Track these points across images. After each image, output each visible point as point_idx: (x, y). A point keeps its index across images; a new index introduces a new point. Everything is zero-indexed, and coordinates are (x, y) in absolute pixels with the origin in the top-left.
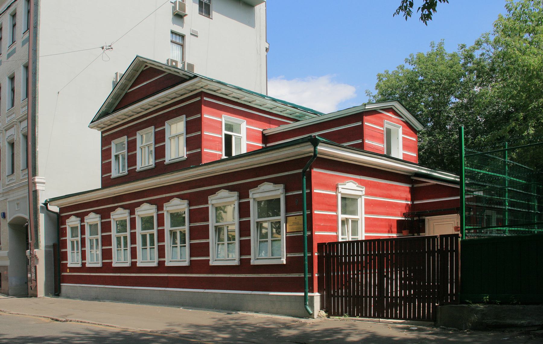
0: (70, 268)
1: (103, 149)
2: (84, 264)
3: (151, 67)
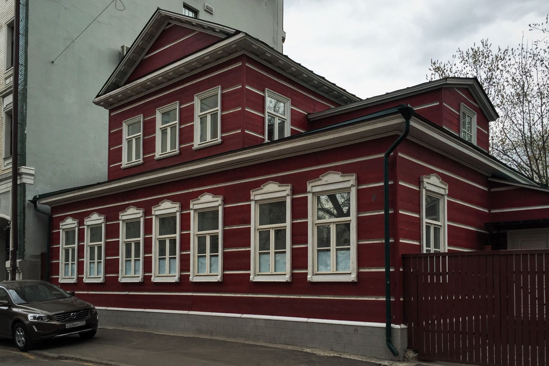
1: (111, 132)
2: (80, 279)
3: (175, 25)
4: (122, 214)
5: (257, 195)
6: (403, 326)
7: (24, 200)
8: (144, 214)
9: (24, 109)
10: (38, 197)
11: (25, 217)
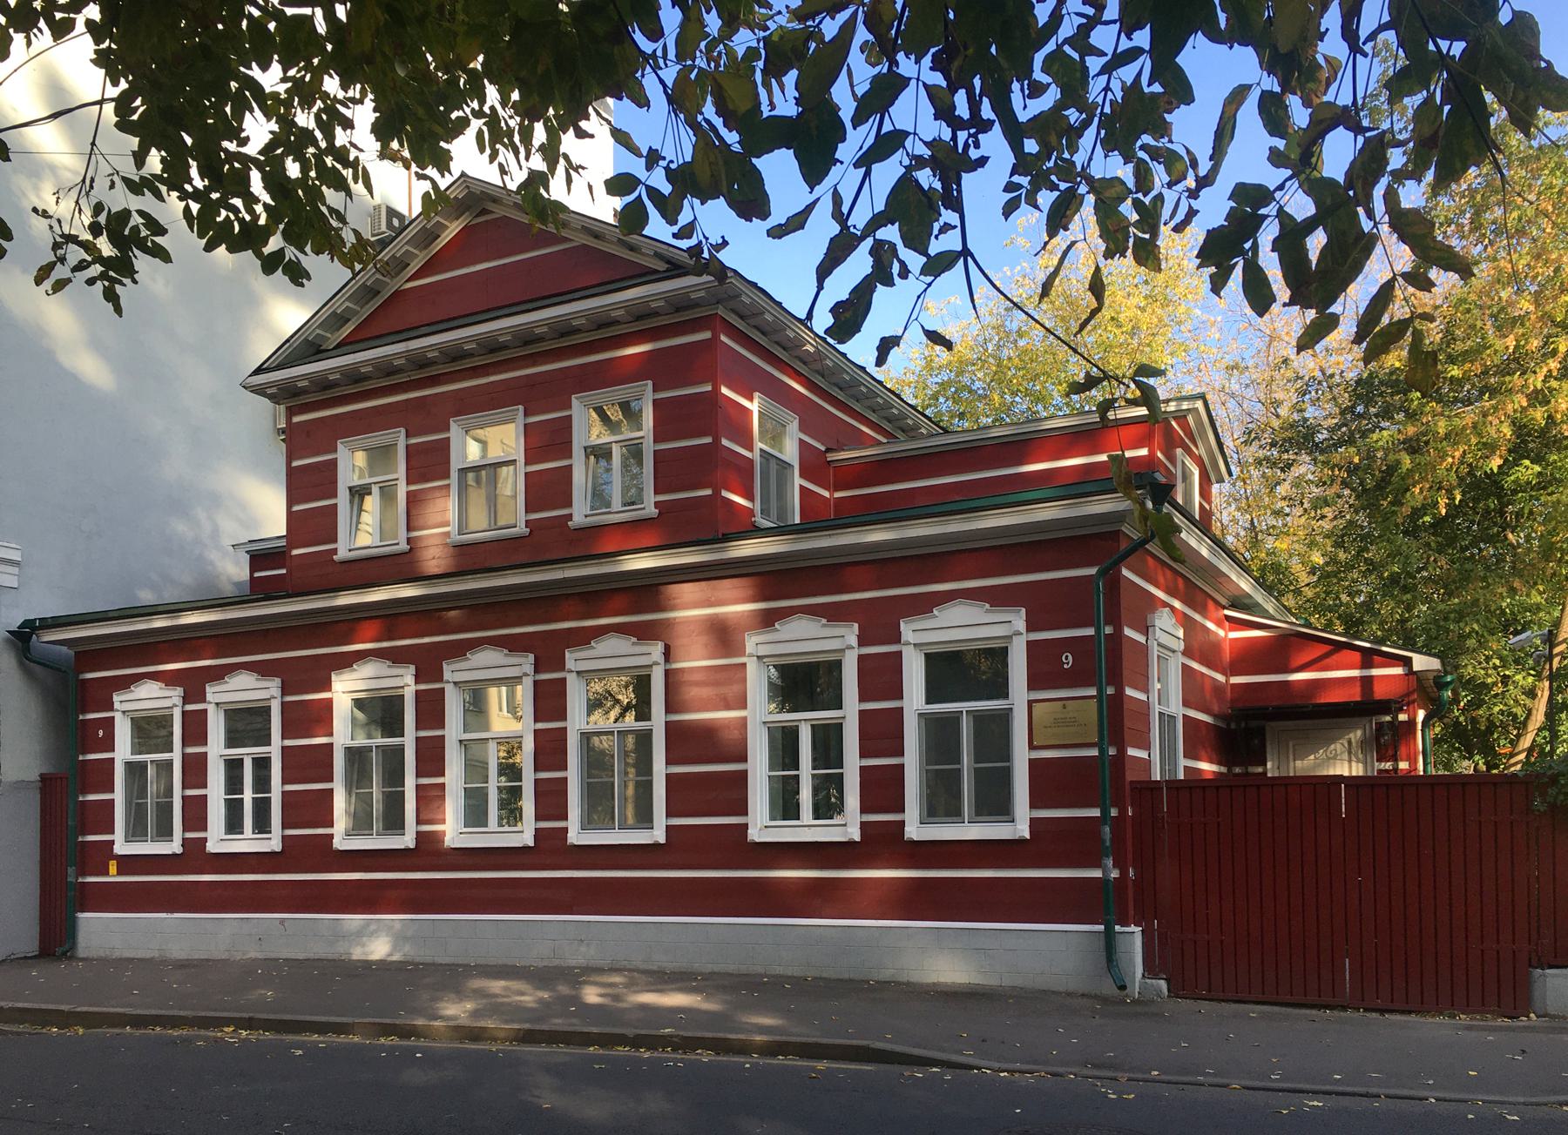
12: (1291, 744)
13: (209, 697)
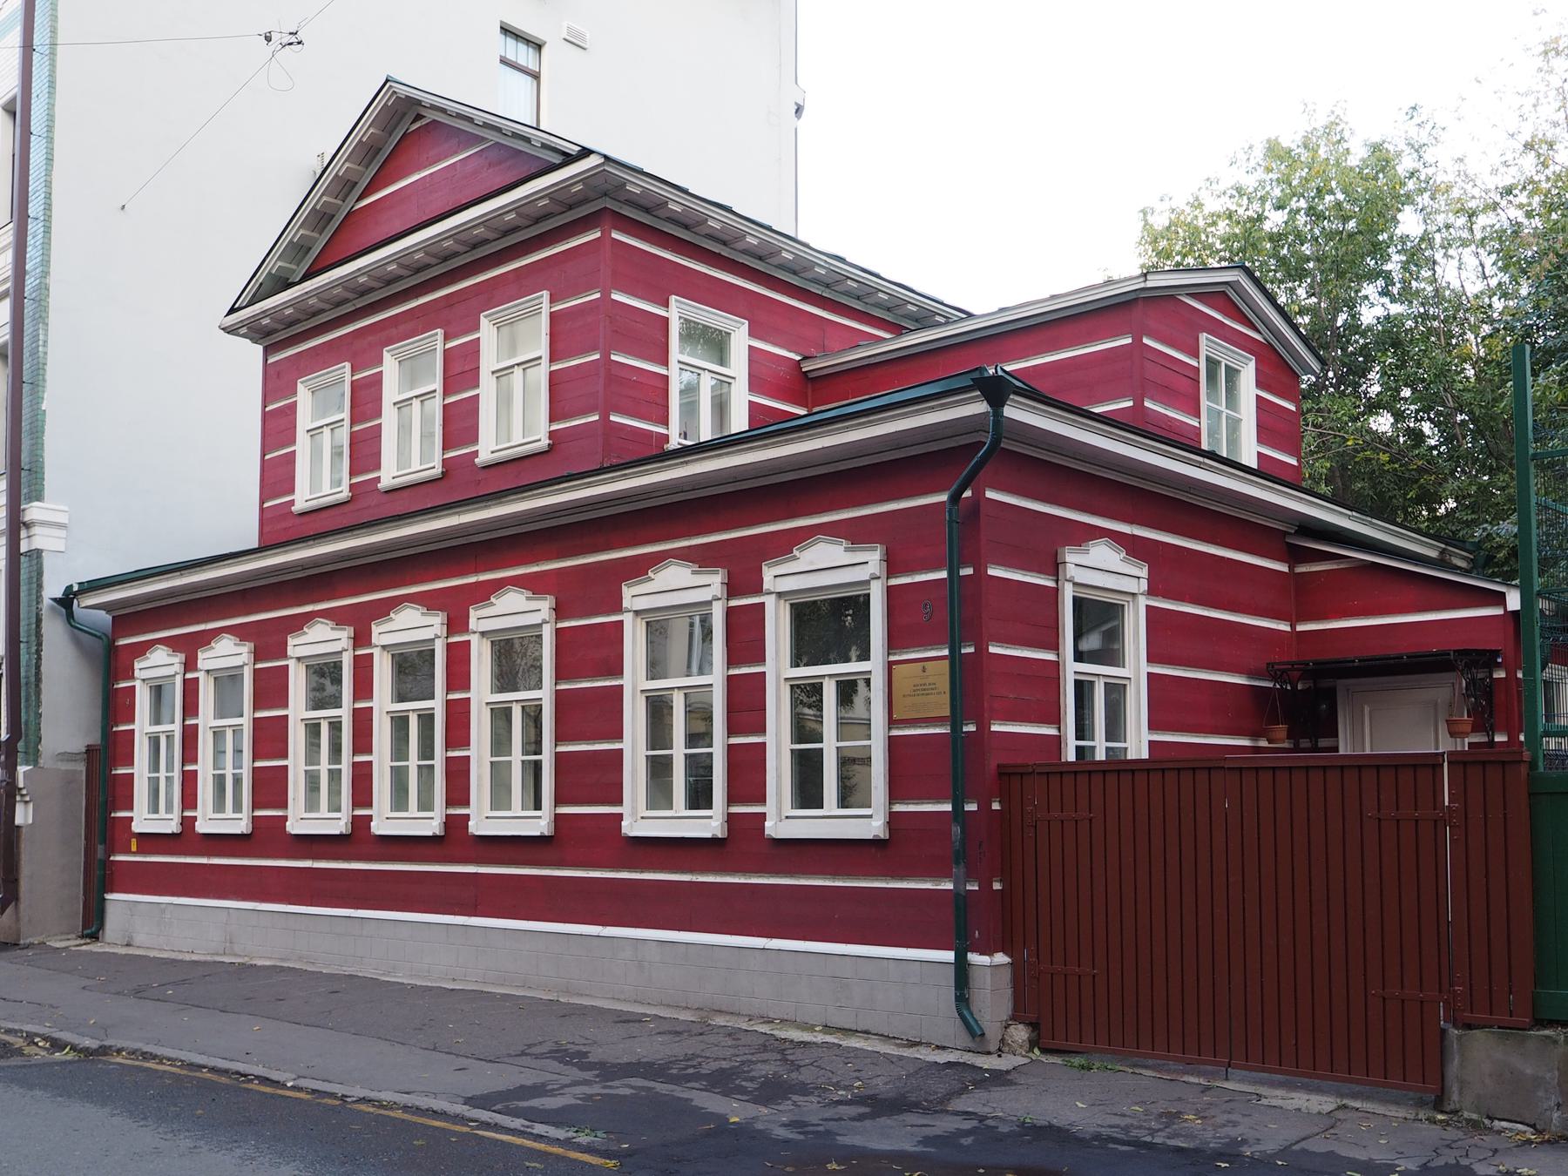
0: (142, 837)
2: (187, 823)
3: (434, 120)
4: (296, 641)
5: (634, 596)
6: (1001, 958)
7: (37, 598)
8: (351, 642)
9: (41, 343)
10: (76, 588)
11: (41, 645)
12: (1367, 709)
13: (473, 624)
